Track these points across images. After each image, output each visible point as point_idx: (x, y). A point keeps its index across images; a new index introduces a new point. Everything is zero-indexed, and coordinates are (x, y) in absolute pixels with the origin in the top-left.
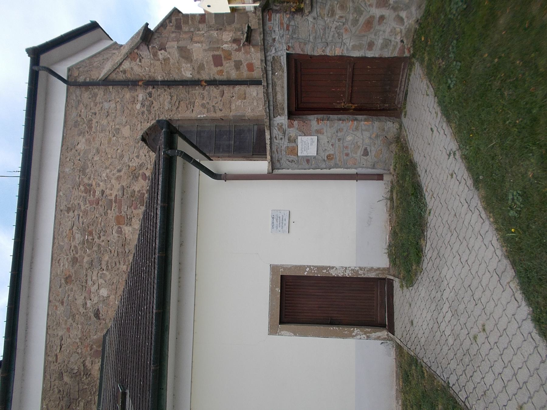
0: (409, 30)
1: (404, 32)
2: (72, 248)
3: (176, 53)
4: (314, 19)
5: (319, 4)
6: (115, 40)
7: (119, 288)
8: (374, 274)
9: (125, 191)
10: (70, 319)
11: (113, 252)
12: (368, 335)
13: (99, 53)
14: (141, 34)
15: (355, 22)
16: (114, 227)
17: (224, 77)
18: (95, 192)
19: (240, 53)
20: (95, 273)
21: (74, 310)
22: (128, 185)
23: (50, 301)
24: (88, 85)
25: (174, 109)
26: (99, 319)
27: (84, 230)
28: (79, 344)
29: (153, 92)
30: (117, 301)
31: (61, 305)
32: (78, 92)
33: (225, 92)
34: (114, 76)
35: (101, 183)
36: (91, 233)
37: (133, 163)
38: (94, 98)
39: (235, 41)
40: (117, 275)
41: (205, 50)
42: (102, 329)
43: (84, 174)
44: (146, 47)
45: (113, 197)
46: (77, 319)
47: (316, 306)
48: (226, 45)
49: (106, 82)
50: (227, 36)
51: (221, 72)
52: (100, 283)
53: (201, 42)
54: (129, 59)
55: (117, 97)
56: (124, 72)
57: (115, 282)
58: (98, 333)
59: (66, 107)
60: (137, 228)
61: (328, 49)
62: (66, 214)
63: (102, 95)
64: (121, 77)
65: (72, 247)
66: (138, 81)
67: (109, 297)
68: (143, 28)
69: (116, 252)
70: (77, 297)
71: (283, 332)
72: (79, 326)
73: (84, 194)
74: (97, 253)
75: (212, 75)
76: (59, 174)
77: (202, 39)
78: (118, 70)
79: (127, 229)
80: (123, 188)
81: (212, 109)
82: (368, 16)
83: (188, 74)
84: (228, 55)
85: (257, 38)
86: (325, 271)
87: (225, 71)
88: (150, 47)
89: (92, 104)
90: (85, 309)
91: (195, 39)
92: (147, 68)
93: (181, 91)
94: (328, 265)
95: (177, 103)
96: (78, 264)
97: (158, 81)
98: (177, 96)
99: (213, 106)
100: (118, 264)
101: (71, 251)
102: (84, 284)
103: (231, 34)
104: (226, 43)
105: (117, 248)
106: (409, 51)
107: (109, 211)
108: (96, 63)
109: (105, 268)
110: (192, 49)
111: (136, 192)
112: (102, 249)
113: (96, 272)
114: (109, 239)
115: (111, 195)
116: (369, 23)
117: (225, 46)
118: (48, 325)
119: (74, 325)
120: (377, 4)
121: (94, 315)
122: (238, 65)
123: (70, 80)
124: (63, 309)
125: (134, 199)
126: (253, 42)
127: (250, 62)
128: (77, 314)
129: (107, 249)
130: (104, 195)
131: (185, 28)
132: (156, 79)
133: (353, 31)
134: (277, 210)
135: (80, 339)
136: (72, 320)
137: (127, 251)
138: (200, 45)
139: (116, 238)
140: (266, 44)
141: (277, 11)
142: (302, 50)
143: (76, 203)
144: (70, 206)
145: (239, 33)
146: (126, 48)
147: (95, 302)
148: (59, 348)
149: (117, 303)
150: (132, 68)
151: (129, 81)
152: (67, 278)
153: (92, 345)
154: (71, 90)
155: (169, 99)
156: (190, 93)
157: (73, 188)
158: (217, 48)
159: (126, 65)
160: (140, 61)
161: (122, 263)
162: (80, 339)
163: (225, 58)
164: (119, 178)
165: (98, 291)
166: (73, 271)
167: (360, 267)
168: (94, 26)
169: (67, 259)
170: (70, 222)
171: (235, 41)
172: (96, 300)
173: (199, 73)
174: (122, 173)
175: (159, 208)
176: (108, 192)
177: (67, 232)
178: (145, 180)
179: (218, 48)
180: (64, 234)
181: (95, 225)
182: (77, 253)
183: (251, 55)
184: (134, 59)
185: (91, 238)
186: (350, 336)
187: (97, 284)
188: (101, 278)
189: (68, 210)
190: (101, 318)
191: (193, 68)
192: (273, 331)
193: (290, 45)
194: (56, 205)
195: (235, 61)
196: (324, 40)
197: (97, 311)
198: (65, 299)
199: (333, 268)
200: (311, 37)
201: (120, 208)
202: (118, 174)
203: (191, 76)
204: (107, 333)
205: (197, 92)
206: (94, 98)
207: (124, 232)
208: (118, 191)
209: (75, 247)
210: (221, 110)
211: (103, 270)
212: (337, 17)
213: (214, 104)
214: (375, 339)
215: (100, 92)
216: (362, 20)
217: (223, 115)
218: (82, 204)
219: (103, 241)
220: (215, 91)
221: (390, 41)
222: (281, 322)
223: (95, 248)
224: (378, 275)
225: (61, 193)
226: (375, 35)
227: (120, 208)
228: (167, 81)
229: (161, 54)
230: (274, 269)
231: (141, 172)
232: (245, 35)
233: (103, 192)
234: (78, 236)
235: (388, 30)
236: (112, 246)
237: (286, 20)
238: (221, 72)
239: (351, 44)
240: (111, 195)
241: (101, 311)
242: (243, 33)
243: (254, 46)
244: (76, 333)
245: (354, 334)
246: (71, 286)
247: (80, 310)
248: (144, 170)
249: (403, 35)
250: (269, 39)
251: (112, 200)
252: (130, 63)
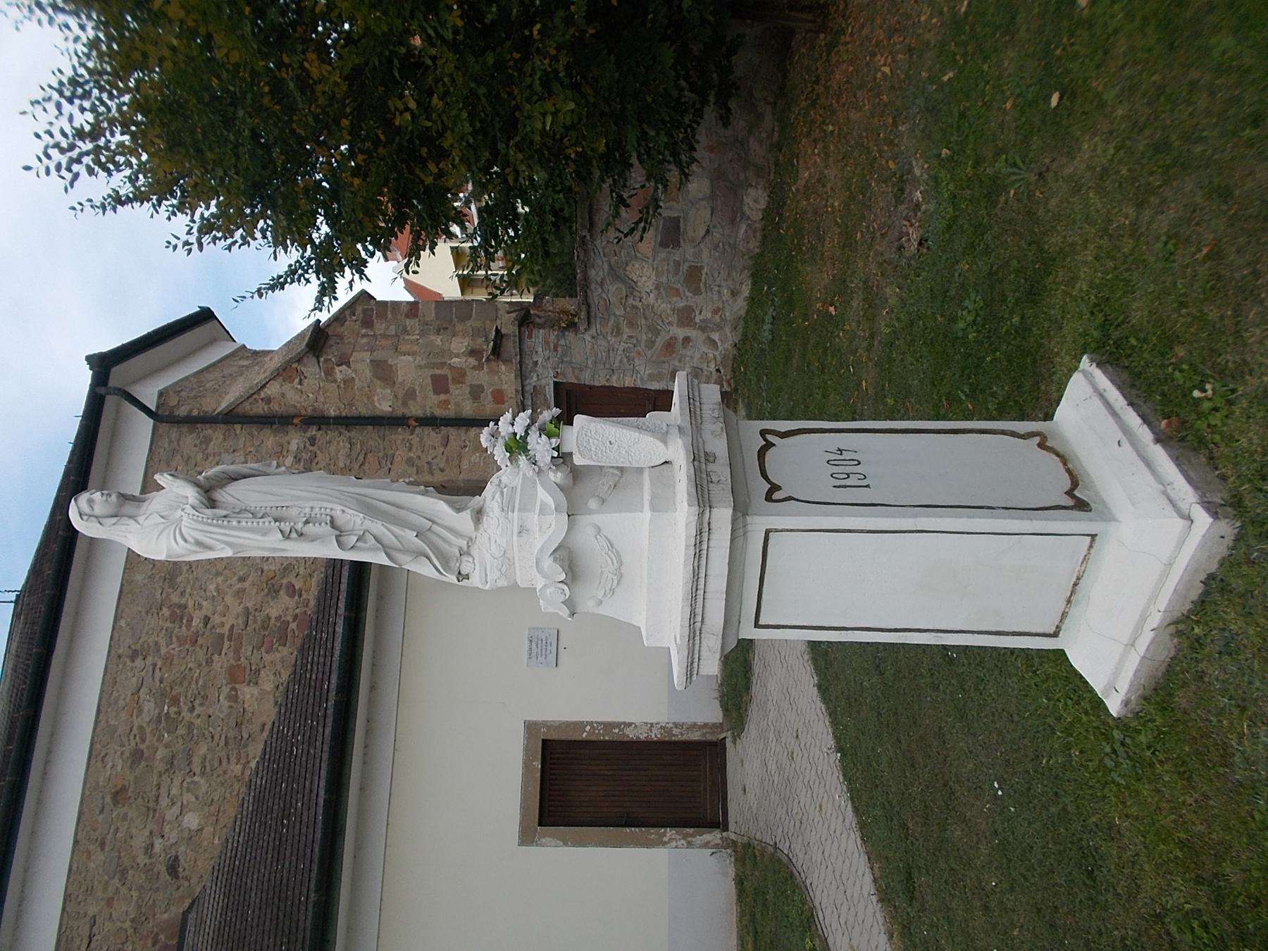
0: (725, 357)
1: (719, 358)
2: (135, 731)
3: (367, 371)
4: (593, 338)
5: (598, 320)
6: (240, 340)
7: (224, 812)
8: (698, 733)
9: (250, 617)
10: (116, 880)
11: (216, 737)
12: (689, 839)
13: (214, 365)
14: (307, 338)
15: (650, 344)
16: (224, 688)
17: (450, 412)
18: (190, 620)
19: (481, 373)
20: (177, 782)
21: (125, 859)
22: (257, 607)
23: (76, 842)
24: (191, 421)
25: (356, 466)
26: (177, 877)
27: (162, 695)
28: (130, 932)
29: (318, 436)
30: (217, 838)
31: (99, 849)
32: (174, 433)
33: (452, 438)
34: (247, 408)
35: (204, 603)
36: (175, 701)
37: (271, 564)
38: (204, 446)
39: (473, 352)
40: (223, 784)
41: (420, 367)
42: (182, 898)
43: (173, 584)
44: (314, 360)
45: (226, 630)
46: (129, 878)
47: (602, 794)
48: (457, 360)
49: (231, 418)
50: (460, 345)
51: (446, 402)
52: (185, 803)
53: (414, 354)
54: (281, 379)
55: (248, 444)
56: (268, 400)
57: (216, 798)
58: (172, 908)
59: (147, 461)
60: (268, 689)
61: (614, 378)
62: (129, 663)
63: (220, 440)
64: (260, 409)
65: (134, 728)
66: (293, 417)
67: (202, 830)
68: (311, 329)
69: (223, 737)
70: (134, 831)
71: (543, 840)
72: (133, 893)
73: (169, 624)
74: (184, 740)
75: (428, 409)
76: (122, 585)
77: (415, 348)
78: (256, 396)
79: (248, 693)
80: (247, 612)
81: (426, 467)
82: (668, 337)
83: (384, 406)
84: (460, 375)
85: (510, 347)
86: (617, 731)
87: (453, 402)
88: (322, 359)
89: (200, 456)
90: (150, 857)
91: (403, 348)
92: (311, 395)
93: (370, 435)
94: (621, 720)
95: (361, 457)
96: (143, 764)
97: (329, 418)
98: (362, 443)
99: (428, 463)
100: (225, 763)
101: (132, 737)
102: (151, 805)
103: (466, 342)
104: (457, 356)
105: (225, 729)
106: (730, 385)
107: (216, 657)
108: (211, 384)
109: (197, 770)
110: (396, 365)
111: (273, 621)
112: (195, 731)
113: (180, 779)
114: (210, 712)
115: (222, 625)
116: (670, 346)
117: (455, 361)
118: (68, 892)
119: (124, 891)
120: (679, 321)
121: (167, 870)
122: (476, 392)
123: (160, 412)
124: (102, 857)
125: (267, 633)
126: (505, 356)
127: (498, 388)
128: (132, 867)
129: (206, 733)
130: (209, 626)
131: (380, 327)
132: (326, 413)
133: (649, 356)
134: (538, 629)
135: (133, 920)
136: (120, 880)
137: (245, 736)
138: (410, 358)
139: (226, 711)
140: (524, 368)
141: (541, 326)
142: (577, 378)
143: (151, 641)
144: (138, 647)
145: (480, 341)
146: (276, 359)
147: (172, 841)
148: (86, 942)
149: (216, 842)
150: (283, 395)
151: (274, 417)
152: (117, 793)
153: (157, 934)
154: (161, 431)
155: (347, 450)
156: (387, 438)
157: (147, 613)
158: (442, 363)
159: (273, 389)
160: (301, 383)
161: (233, 760)
162: (133, 920)
163: (453, 379)
164: (240, 594)
165: (180, 818)
166: (131, 778)
167: (674, 723)
168: (205, 316)
169: (122, 754)
170: (135, 680)
171: (473, 352)
172: (173, 836)
173: (405, 404)
174: (247, 584)
175: (340, 622)
176: (216, 619)
177: (128, 699)
178: (292, 596)
179: (443, 364)
180: (121, 703)
181: (185, 684)
182: (143, 741)
183: (499, 377)
184: (290, 379)
185: (176, 709)
186: (661, 843)
187: (180, 804)
188: (188, 790)
189: (134, 655)
190: (181, 876)
191: (396, 396)
192: (527, 838)
193: (559, 371)
194: (110, 646)
195: (471, 386)
196: (607, 366)
197: (174, 861)
198: (109, 837)
199: (630, 724)
200: (589, 362)
201: (237, 651)
202: (240, 585)
203: (390, 409)
204: (191, 907)
205: (401, 437)
206: (204, 446)
207: (241, 697)
208: (237, 618)
209: (141, 728)
210: (442, 470)
211: (194, 774)
212: (625, 336)
213: (430, 459)
214: (700, 847)
215: (216, 435)
216: (660, 341)
217: (446, 478)
218: (163, 642)
219: (199, 716)
220: (432, 436)
221: (702, 370)
222: (541, 823)
223: (181, 731)
224: (704, 735)
225: (122, 623)
226: (680, 361)
227: (237, 651)
228: (346, 417)
229: (340, 373)
230: (531, 727)
231: (285, 581)
232: (492, 343)
233: (207, 620)
234: (149, 707)
235: (697, 355)
236: (216, 724)
237: (553, 337)
238: (446, 402)
239: (647, 372)
240: (222, 625)
241: (182, 861)
242: (487, 341)
243: (504, 362)
244: (125, 909)
245: (666, 839)
246: (125, 809)
247: (139, 860)
248: (291, 578)
249: (718, 362)
250: (529, 362)
251: (223, 635)
252: (282, 386)
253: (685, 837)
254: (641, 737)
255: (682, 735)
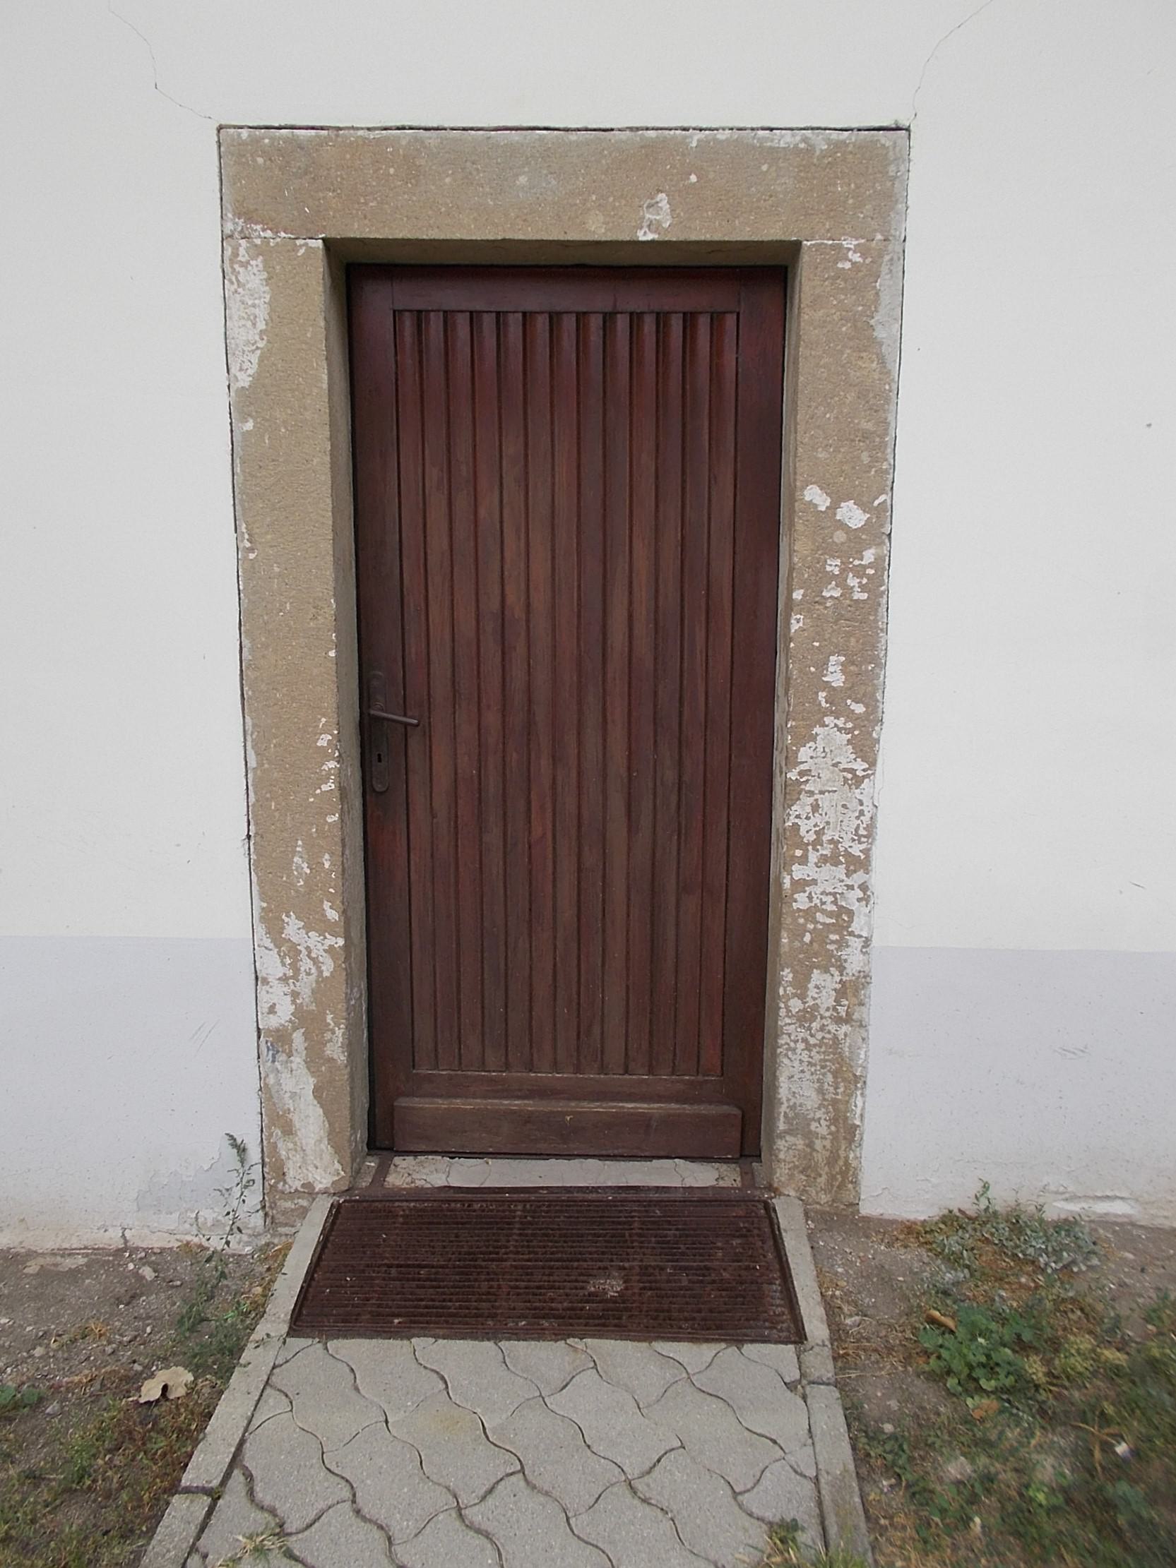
12: (298, 1038)
71: (254, 277)
86: (835, 677)
199: (866, 748)
214: (266, 1093)
245: (293, 928)
253: (302, 1017)
254: (800, 808)
255: (806, 1017)
